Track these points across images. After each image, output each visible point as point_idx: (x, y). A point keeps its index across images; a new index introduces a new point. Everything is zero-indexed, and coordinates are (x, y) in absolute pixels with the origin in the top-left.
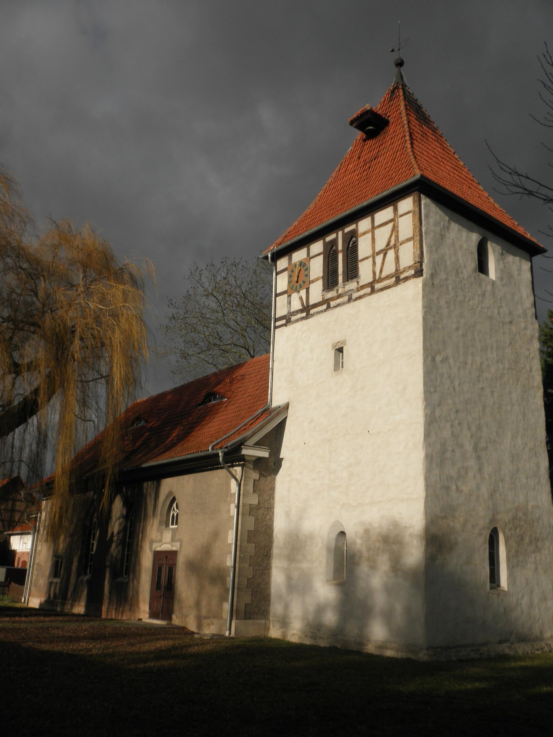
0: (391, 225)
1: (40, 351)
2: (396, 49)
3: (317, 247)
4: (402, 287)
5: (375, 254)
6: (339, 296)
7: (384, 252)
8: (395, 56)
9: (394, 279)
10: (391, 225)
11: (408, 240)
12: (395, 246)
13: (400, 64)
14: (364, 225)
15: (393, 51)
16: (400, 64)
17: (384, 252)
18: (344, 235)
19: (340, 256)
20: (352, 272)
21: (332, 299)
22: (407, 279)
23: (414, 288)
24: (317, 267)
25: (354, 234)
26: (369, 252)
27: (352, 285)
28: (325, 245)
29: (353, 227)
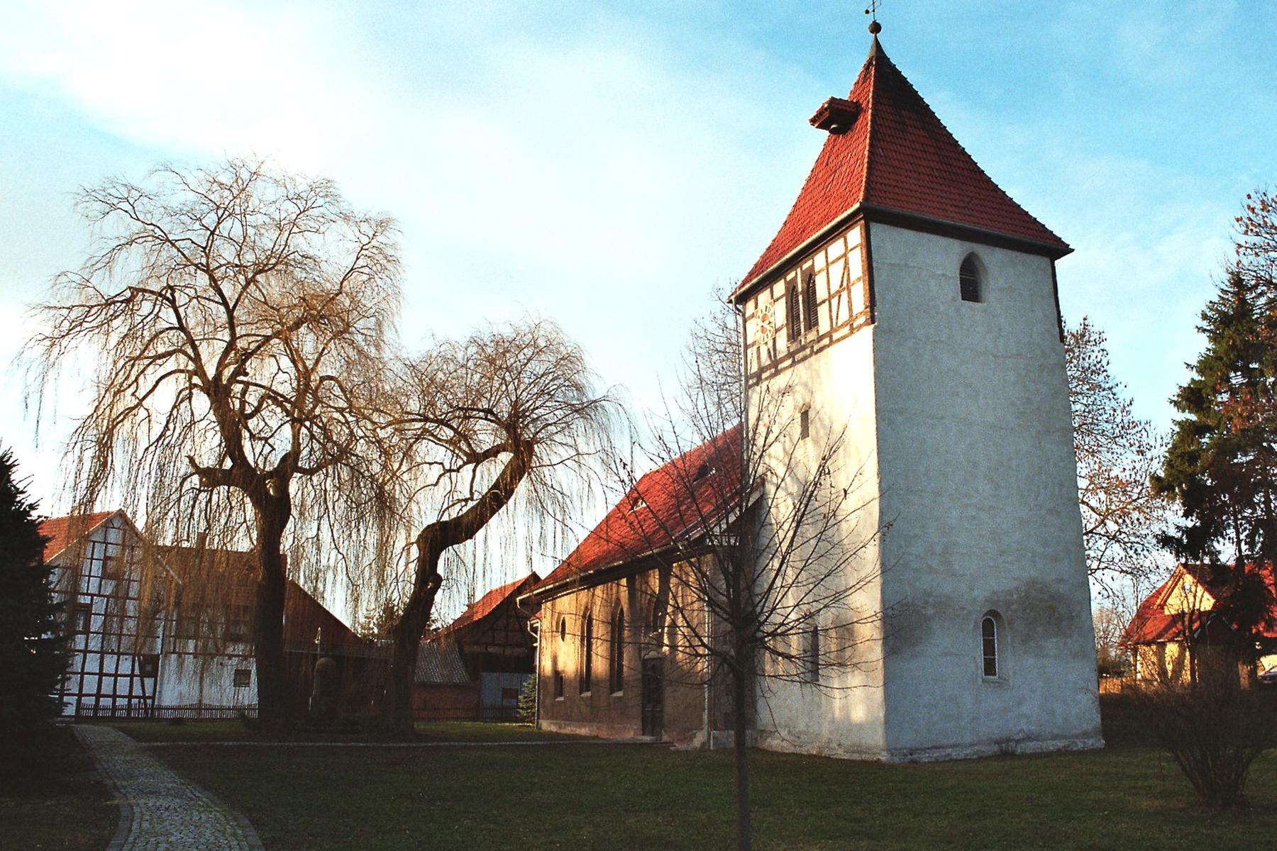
0: (842, 260)
1: (1156, 803)
2: (871, 10)
3: (780, 288)
4: (857, 335)
5: (830, 297)
6: (804, 348)
7: (839, 293)
8: (869, 20)
9: (855, 325)
10: (842, 260)
11: (859, 279)
12: (848, 288)
13: (876, 28)
14: (819, 260)
15: (867, 12)
16: (876, 28)
17: (839, 293)
18: (802, 272)
19: (800, 298)
20: (812, 322)
21: (798, 351)
22: (860, 327)
23: (866, 335)
24: (780, 310)
25: (810, 278)
26: (826, 296)
27: (812, 336)
28: (787, 283)
29: (809, 263)
